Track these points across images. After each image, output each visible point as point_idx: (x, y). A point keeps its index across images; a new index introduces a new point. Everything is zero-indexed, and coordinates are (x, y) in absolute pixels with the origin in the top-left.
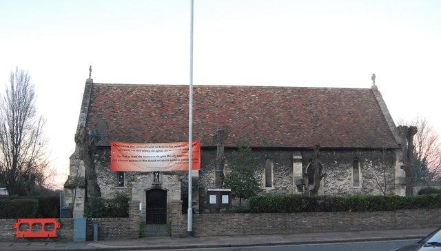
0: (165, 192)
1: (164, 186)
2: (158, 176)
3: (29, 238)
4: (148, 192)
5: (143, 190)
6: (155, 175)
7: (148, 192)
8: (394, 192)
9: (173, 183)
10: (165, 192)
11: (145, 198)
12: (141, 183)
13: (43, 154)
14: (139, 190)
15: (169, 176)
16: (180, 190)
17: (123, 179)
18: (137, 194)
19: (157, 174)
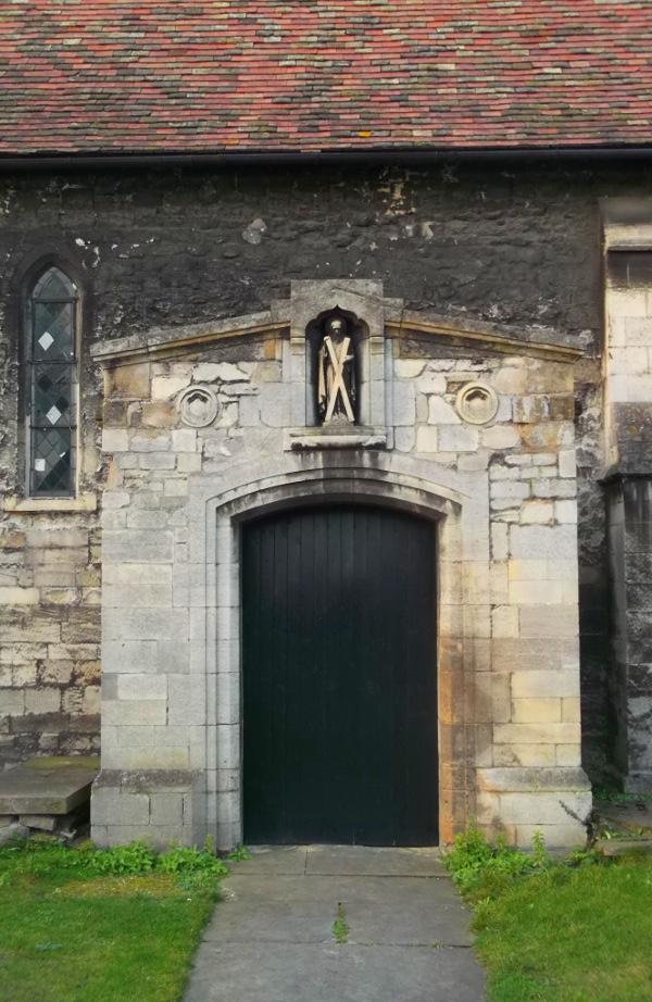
0: (420, 526)
1: (411, 472)
2: (353, 373)
3: (428, 493)
4: (258, 530)
5: (201, 509)
6: (318, 364)
7: (258, 530)
8: (641, 656)
9: (506, 438)
10: (420, 526)
11: (229, 592)
12: (184, 440)
13: (121, 792)
14: (172, 506)
15: (462, 368)
16: (569, 513)
17: (65, 430)
18: (147, 545)
19: (339, 352)
